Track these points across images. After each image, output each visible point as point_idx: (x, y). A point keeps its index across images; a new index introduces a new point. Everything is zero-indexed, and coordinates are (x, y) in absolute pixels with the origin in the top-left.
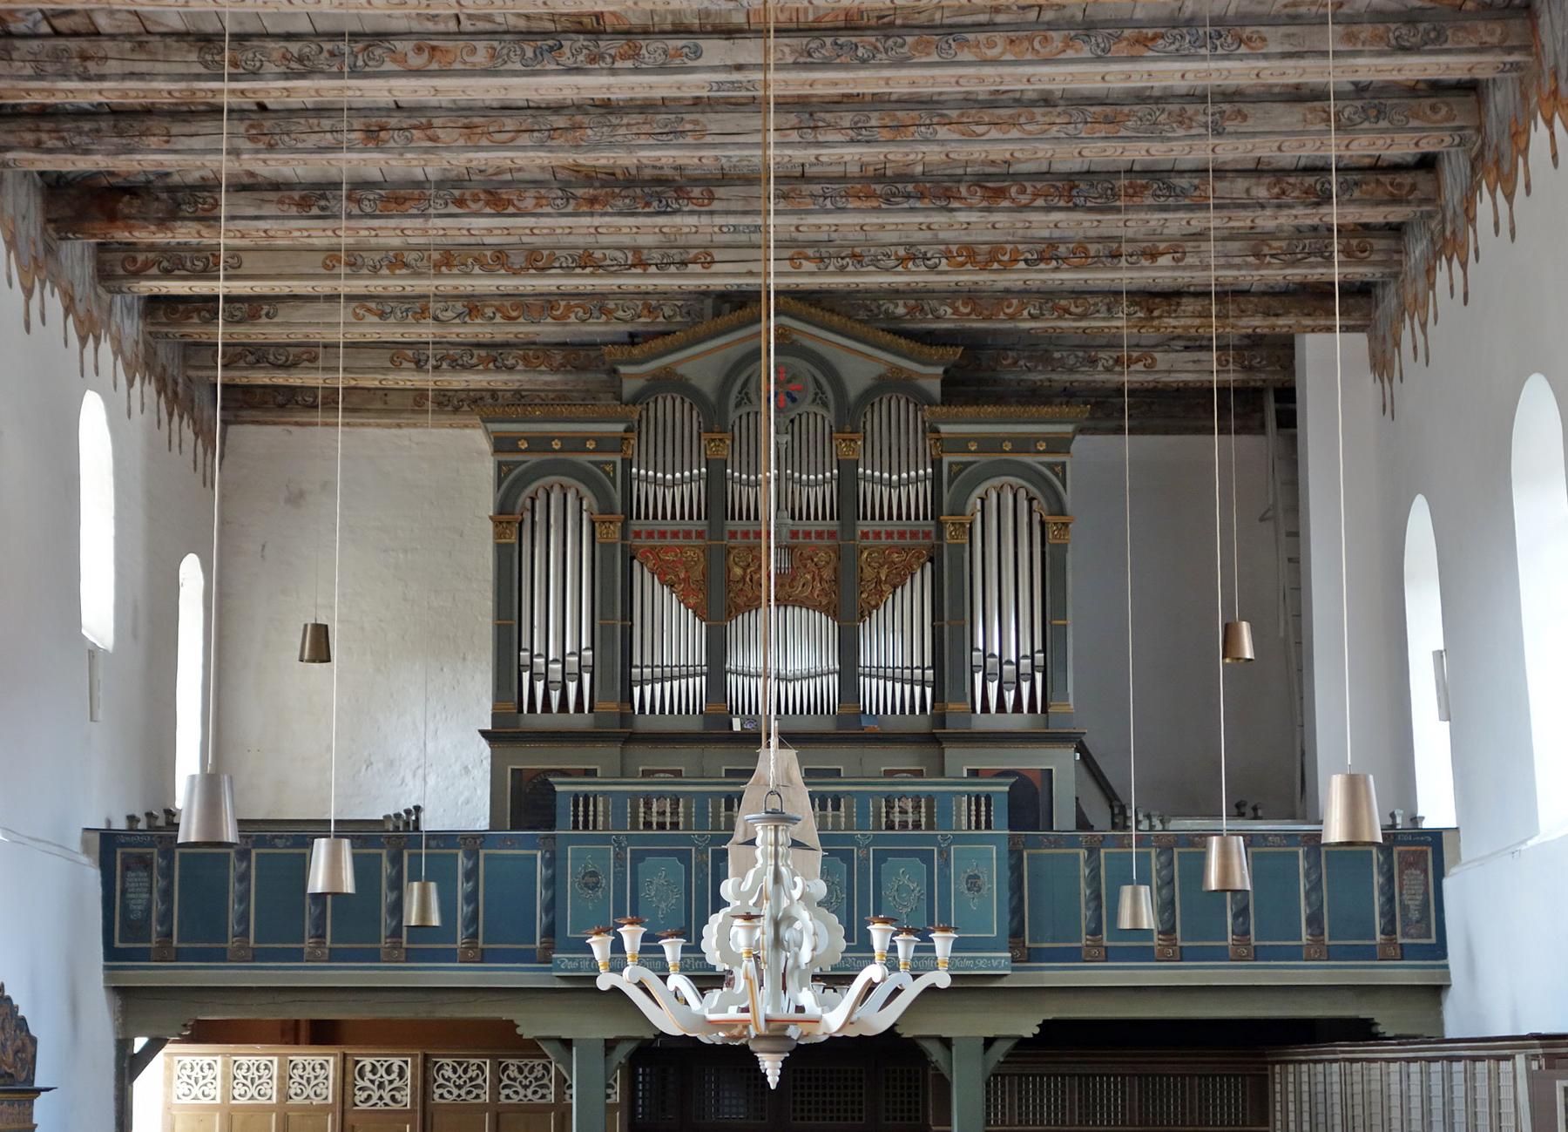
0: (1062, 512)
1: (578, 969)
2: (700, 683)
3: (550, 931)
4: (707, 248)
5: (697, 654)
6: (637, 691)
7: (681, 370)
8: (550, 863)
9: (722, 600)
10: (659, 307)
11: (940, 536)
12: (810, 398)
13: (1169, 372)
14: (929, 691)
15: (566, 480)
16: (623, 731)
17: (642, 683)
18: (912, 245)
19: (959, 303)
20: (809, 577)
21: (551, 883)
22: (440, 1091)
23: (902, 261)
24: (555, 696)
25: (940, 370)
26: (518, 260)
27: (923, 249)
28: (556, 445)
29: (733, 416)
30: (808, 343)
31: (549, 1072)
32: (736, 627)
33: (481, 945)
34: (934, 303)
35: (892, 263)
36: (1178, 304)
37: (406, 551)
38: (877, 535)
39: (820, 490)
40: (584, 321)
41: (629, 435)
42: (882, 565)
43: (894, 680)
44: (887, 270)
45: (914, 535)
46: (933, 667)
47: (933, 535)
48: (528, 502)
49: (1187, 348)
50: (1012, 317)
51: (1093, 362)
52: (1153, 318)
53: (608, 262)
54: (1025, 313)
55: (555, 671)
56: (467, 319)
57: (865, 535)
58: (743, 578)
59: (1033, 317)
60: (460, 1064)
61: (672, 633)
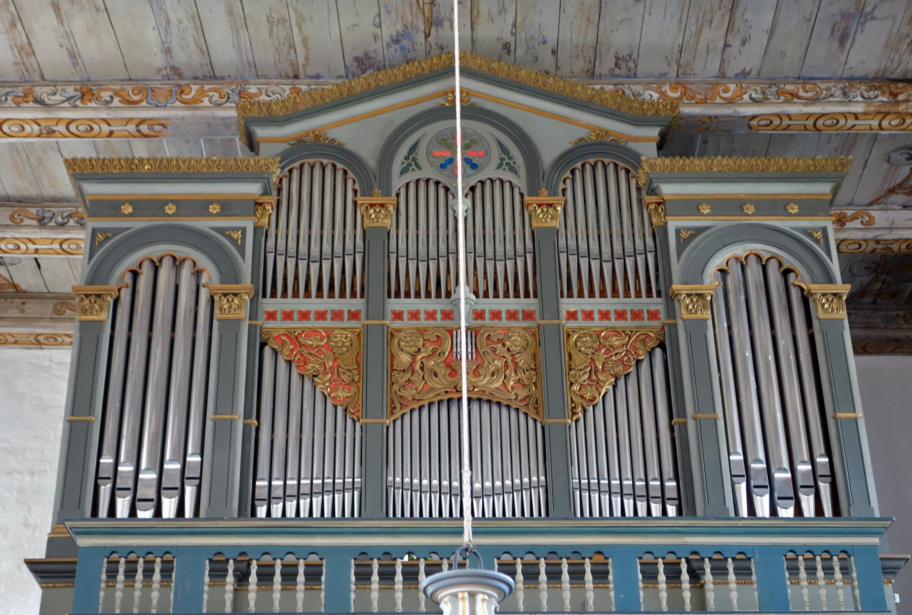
7: (332, 134)
11: (671, 313)
12: (495, 161)
13: (891, 229)
19: (666, 88)
25: (655, 132)
29: (398, 183)
37: (33, 474)
38: (589, 315)
40: (219, 105)
41: (265, 199)
47: (662, 315)
48: (128, 279)
50: (730, 102)
52: (898, 103)
54: (746, 97)
56: (78, 103)
57: (572, 315)
58: (412, 365)
59: (754, 101)
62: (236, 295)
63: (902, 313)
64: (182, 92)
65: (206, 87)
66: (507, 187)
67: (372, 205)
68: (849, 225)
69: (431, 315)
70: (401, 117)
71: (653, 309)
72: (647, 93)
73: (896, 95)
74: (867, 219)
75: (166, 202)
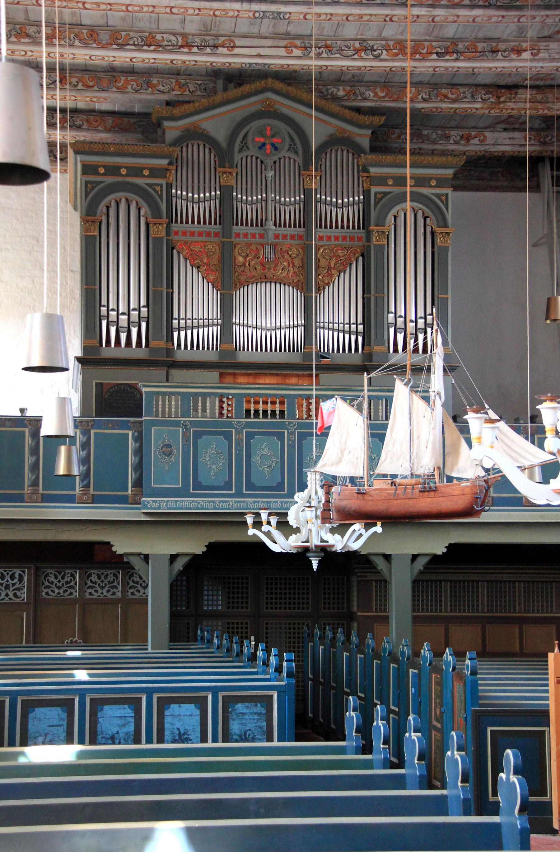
0: (446, 226)
1: (159, 508)
2: (215, 331)
3: (138, 483)
4: (231, 36)
5: (215, 313)
6: (176, 334)
8: (139, 439)
9: (228, 280)
10: (186, 84)
11: (368, 239)
12: (287, 147)
13: (494, 145)
14: (360, 339)
15: (130, 196)
16: (166, 362)
17: (179, 330)
18: (365, 40)
19: (378, 90)
20: (286, 264)
21: (139, 452)
22: (46, 590)
23: (357, 51)
24: (123, 336)
25: (369, 132)
26: (105, 37)
27: (371, 43)
28: (124, 171)
30: (285, 111)
31: (117, 578)
32: (239, 296)
33: (92, 492)
34: (363, 89)
35: (351, 52)
36: (516, 93)
38: (329, 238)
39: (292, 208)
40: (137, 91)
41: (170, 167)
42: (331, 258)
43: (338, 331)
44: (348, 57)
45: (352, 239)
46: (363, 323)
47: (364, 240)
48: (105, 210)
49: (505, 130)
51: (448, 137)
53: (166, 43)
54: (420, 97)
55: (123, 320)
58: (244, 264)
59: (424, 100)
60: (60, 573)
61: (196, 301)
62: (160, 224)
63: (501, 170)
64: (116, 81)
65: (129, 78)
66: (292, 161)
67: (225, 173)
68: (472, 142)
69: (253, 236)
70: (239, 116)
71: (360, 235)
72: (368, 92)
73: (499, 98)
74: (482, 138)
75: (120, 168)
